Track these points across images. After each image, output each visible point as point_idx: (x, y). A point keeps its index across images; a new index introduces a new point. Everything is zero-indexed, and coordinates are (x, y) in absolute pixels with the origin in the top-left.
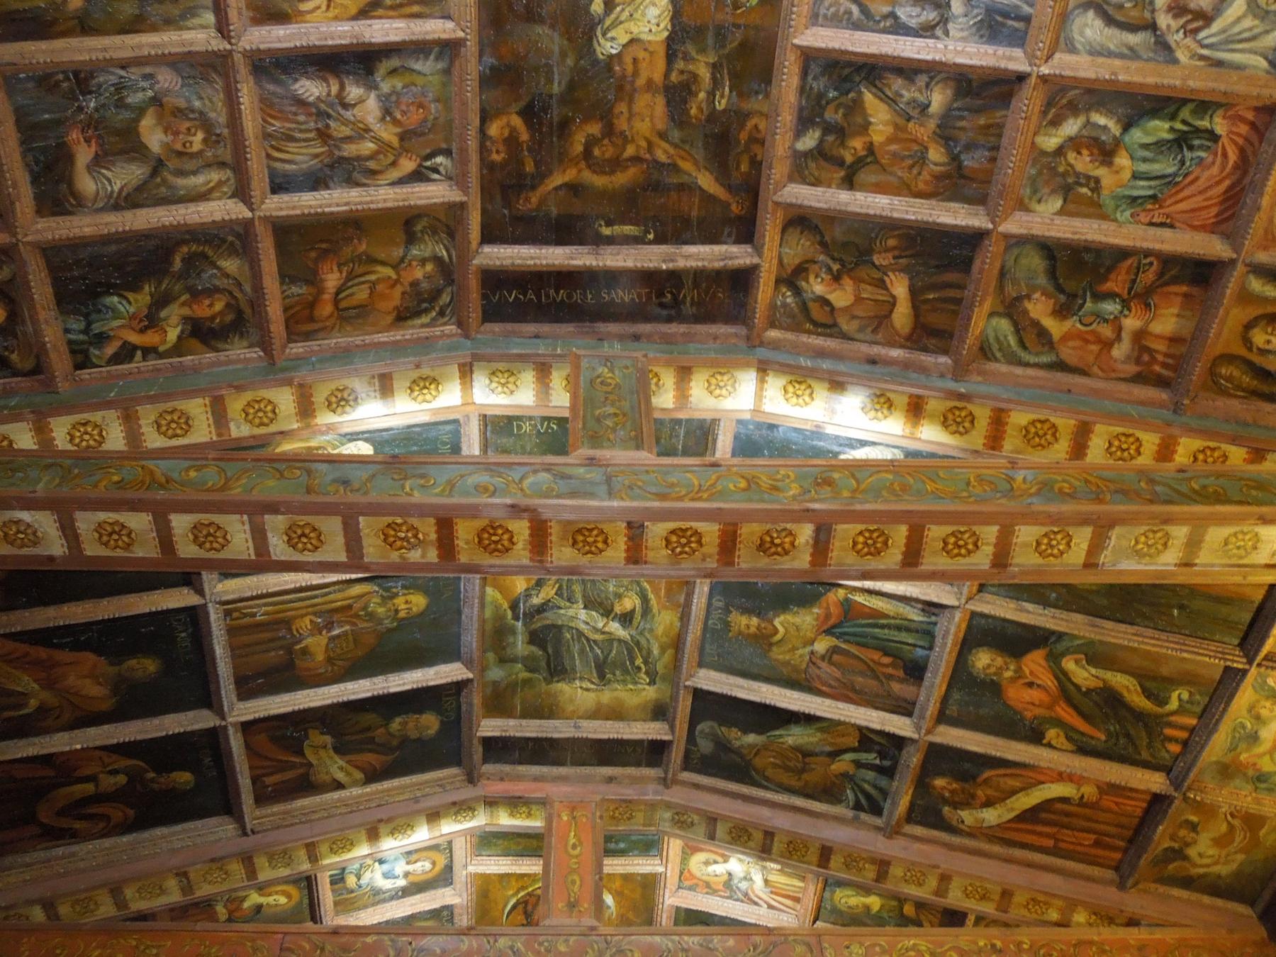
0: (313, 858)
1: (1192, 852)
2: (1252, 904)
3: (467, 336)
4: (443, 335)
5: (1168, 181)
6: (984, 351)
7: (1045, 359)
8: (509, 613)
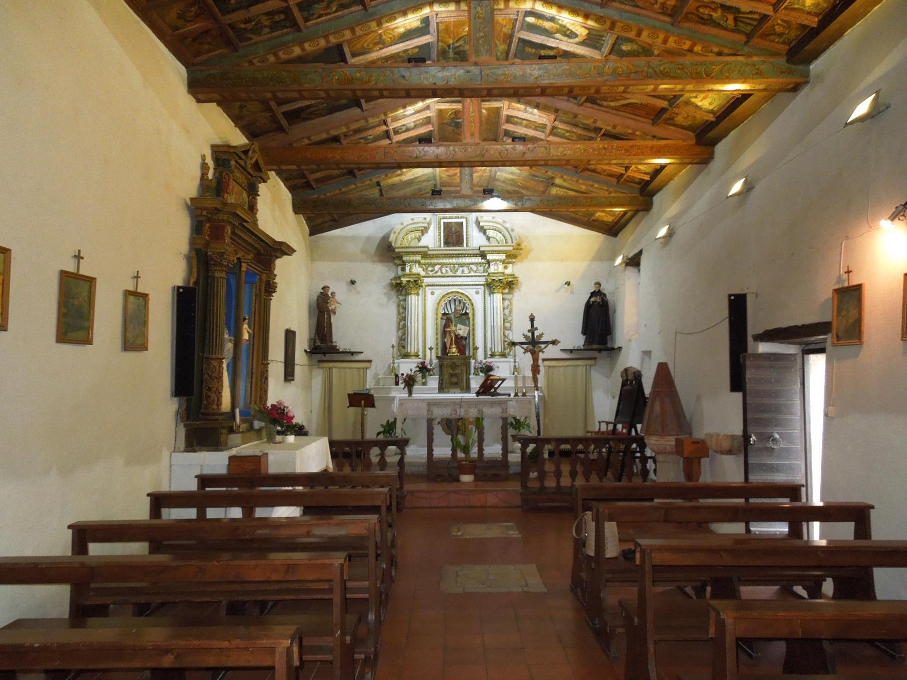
0: (385, 114)
1: (676, 119)
2: (694, 132)
7: (632, 4)
8: (447, 48)
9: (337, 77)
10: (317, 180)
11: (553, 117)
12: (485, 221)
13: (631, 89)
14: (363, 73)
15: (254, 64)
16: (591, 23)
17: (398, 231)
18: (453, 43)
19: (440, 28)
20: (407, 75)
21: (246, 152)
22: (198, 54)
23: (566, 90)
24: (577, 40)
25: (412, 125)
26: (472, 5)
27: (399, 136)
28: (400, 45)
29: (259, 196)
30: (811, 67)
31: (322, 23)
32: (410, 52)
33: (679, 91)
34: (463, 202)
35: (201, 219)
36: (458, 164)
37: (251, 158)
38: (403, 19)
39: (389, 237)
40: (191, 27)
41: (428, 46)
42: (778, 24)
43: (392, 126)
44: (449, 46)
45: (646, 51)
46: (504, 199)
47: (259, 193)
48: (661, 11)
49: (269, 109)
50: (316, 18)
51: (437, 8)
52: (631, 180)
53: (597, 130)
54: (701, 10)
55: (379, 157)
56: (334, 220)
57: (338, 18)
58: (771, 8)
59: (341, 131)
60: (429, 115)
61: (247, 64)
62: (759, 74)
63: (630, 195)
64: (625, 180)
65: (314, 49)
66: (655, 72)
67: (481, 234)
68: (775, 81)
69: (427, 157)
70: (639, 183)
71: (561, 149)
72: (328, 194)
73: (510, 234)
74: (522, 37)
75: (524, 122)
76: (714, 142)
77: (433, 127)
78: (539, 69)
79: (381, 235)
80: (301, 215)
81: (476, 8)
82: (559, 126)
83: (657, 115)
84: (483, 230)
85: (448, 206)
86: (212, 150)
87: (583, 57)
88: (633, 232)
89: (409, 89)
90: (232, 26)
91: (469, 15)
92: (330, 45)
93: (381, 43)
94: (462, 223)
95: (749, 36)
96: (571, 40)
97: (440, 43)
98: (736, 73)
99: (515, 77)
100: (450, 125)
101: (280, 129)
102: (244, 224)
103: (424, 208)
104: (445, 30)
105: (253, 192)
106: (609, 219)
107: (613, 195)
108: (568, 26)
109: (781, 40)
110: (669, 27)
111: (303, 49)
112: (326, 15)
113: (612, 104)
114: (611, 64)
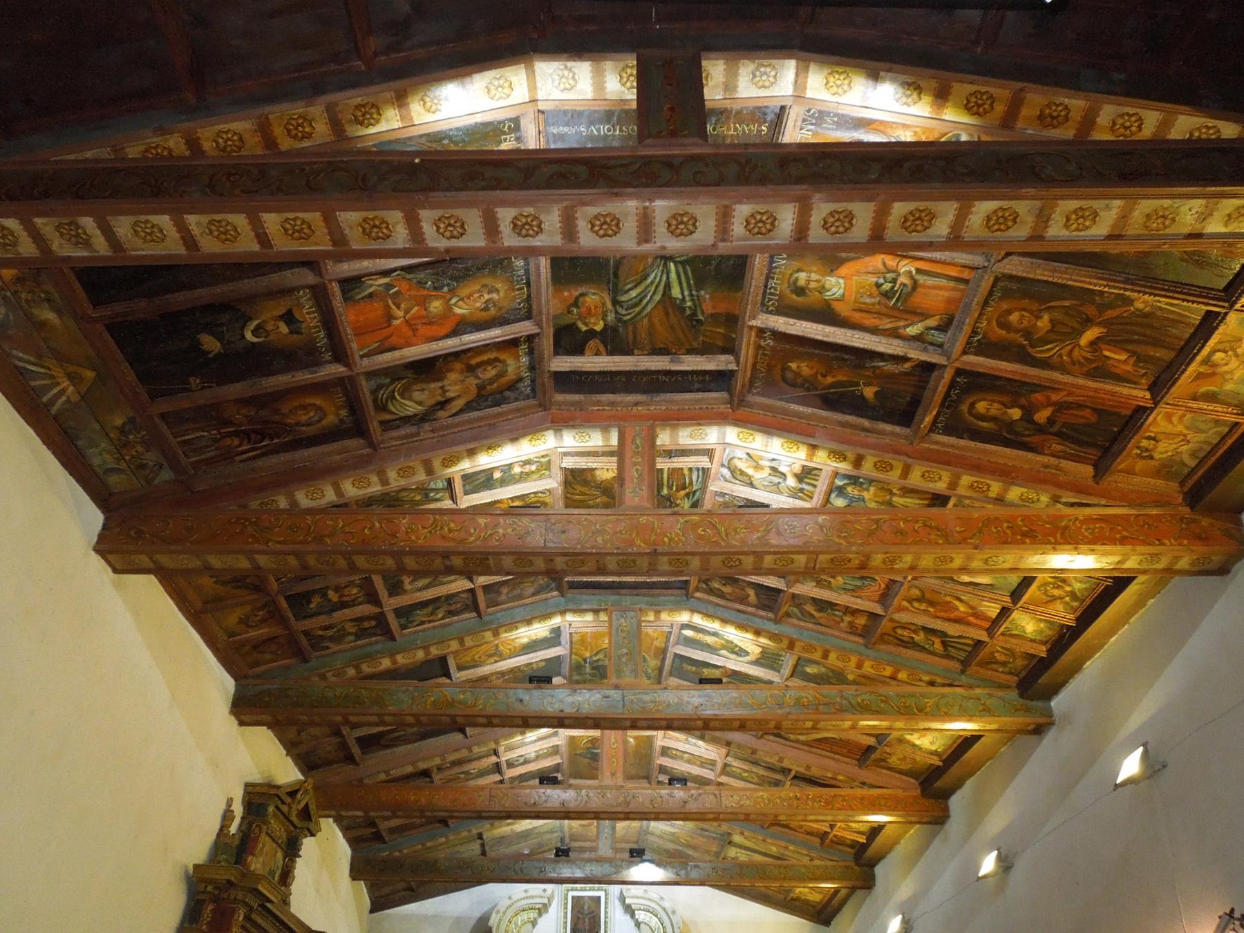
0: (497, 742)
1: (889, 761)
3: (562, 596)
4: (553, 597)
5: (859, 587)
6: (787, 615)
9: (433, 699)
10: (392, 831)
11: (724, 751)
12: (633, 897)
13: (822, 724)
14: (468, 694)
15: (326, 679)
16: (763, 640)
17: (502, 911)
18: (591, 657)
19: (574, 639)
20: (526, 698)
21: (293, 794)
22: (257, 664)
23: (737, 724)
24: (748, 658)
25: (533, 755)
26: (614, 617)
27: (514, 770)
28: (522, 657)
29: (300, 856)
30: (1052, 704)
31: (424, 630)
32: (535, 666)
33: (887, 729)
34: (599, 868)
35: (203, 897)
36: (592, 816)
37: (299, 802)
38: (527, 629)
39: (488, 919)
40: (253, 634)
41: (558, 659)
42: (998, 651)
43: (505, 757)
44: (585, 660)
45: (837, 677)
46: (659, 864)
47: (300, 853)
48: (849, 630)
49: (338, 733)
50: (418, 625)
51: (569, 617)
52: (840, 842)
53: (785, 771)
54: (899, 631)
55: (481, 802)
56: (411, 889)
57: (445, 625)
58: (985, 633)
59: (434, 763)
60: (556, 743)
61: (317, 679)
62: (986, 711)
63: (840, 864)
64: (832, 841)
65: (408, 661)
66: (851, 704)
67: (628, 917)
68: (1009, 721)
69: (549, 805)
70: (851, 846)
71: (736, 798)
72: (405, 851)
73: (669, 918)
74: (678, 652)
75: (686, 756)
76: (947, 794)
77: (562, 758)
78: (700, 696)
79: (477, 914)
80: (362, 882)
81: (618, 620)
82: (734, 764)
83: (863, 754)
84: (630, 910)
85: (579, 874)
86: (245, 790)
87: (758, 680)
88: (852, 920)
89: (527, 717)
90: (306, 633)
91: (610, 626)
92: (430, 657)
93: (499, 656)
94: (599, 898)
95: (965, 664)
96: (741, 659)
97: (573, 656)
98: (956, 708)
99: (669, 705)
100: (586, 758)
101: (350, 759)
102: (268, 905)
103: (542, 876)
104: (579, 641)
105: (292, 850)
106: (816, 897)
107: (817, 862)
108: (736, 642)
109: (1007, 670)
110: (862, 649)
111: (394, 662)
112: (430, 622)
113: (802, 738)
114: (792, 693)
